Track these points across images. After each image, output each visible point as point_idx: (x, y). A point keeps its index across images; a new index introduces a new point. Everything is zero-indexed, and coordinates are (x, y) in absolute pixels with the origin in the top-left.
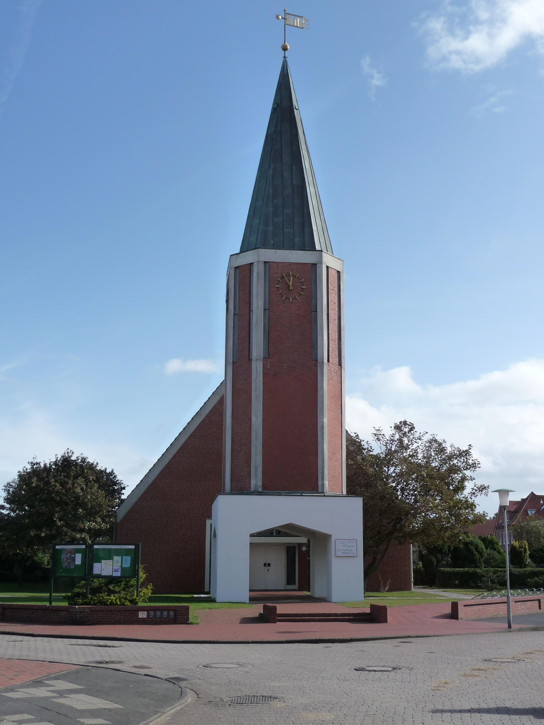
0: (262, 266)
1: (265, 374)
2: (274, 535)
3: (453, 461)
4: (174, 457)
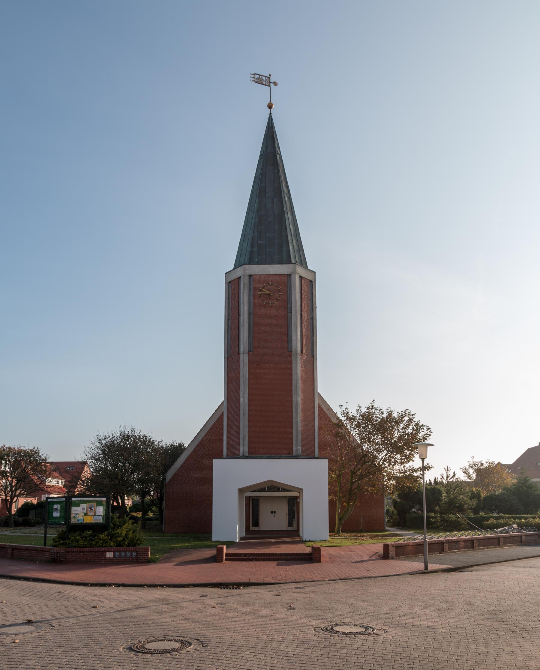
0: (247, 279)
1: (250, 364)
2: (266, 490)
3: (408, 430)
4: (206, 435)
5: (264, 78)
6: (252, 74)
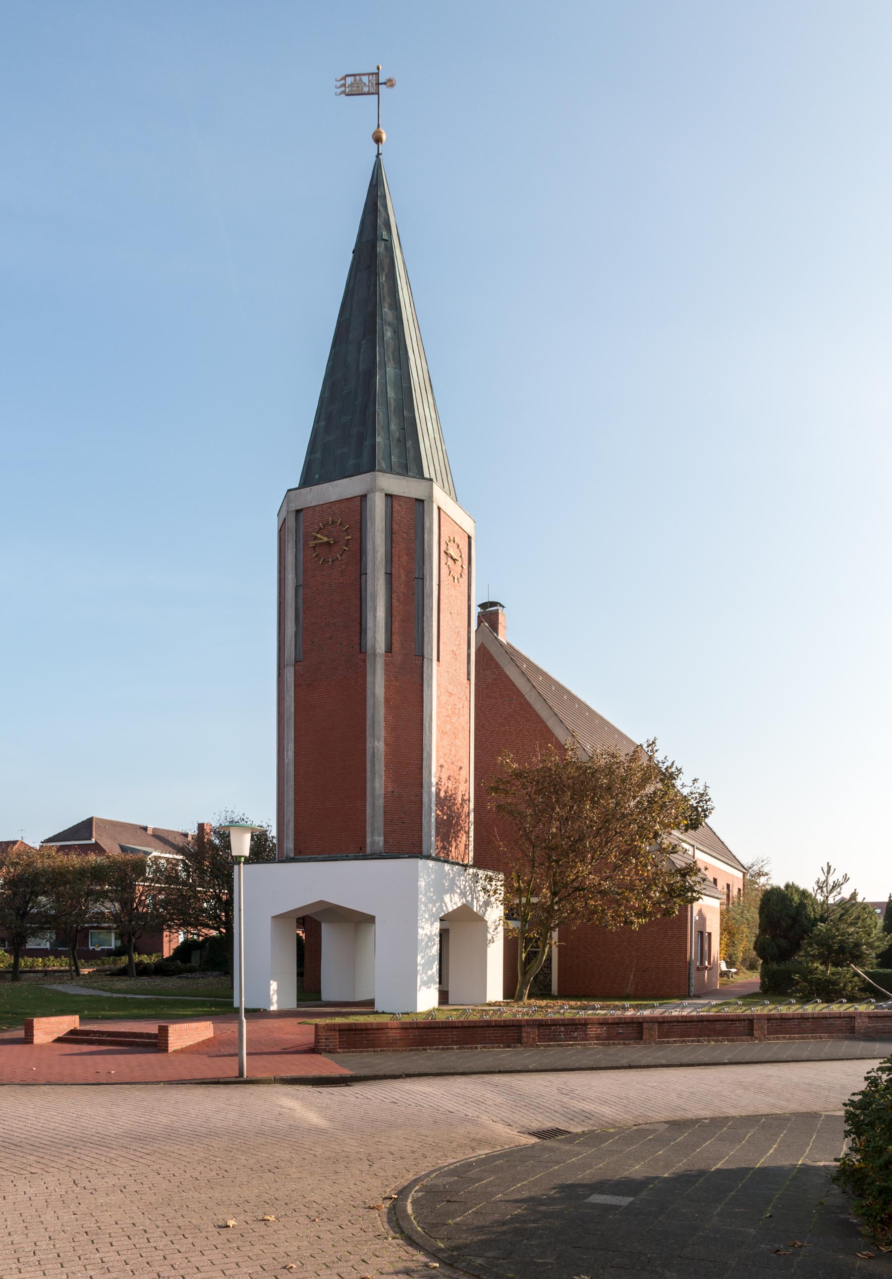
5: (365, 79)
6: (339, 79)
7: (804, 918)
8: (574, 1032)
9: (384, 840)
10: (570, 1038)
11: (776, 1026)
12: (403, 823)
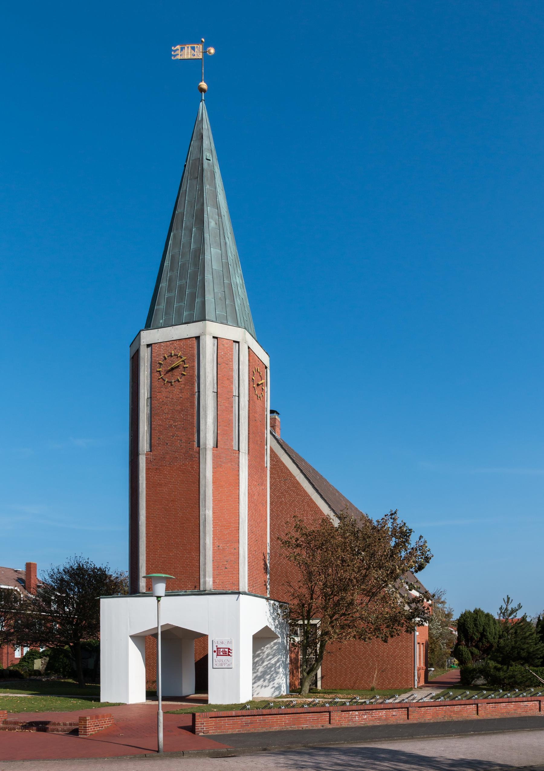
7: (488, 634)
8: (364, 715)
9: (213, 581)
10: (362, 719)
11: (492, 708)
12: (226, 568)
